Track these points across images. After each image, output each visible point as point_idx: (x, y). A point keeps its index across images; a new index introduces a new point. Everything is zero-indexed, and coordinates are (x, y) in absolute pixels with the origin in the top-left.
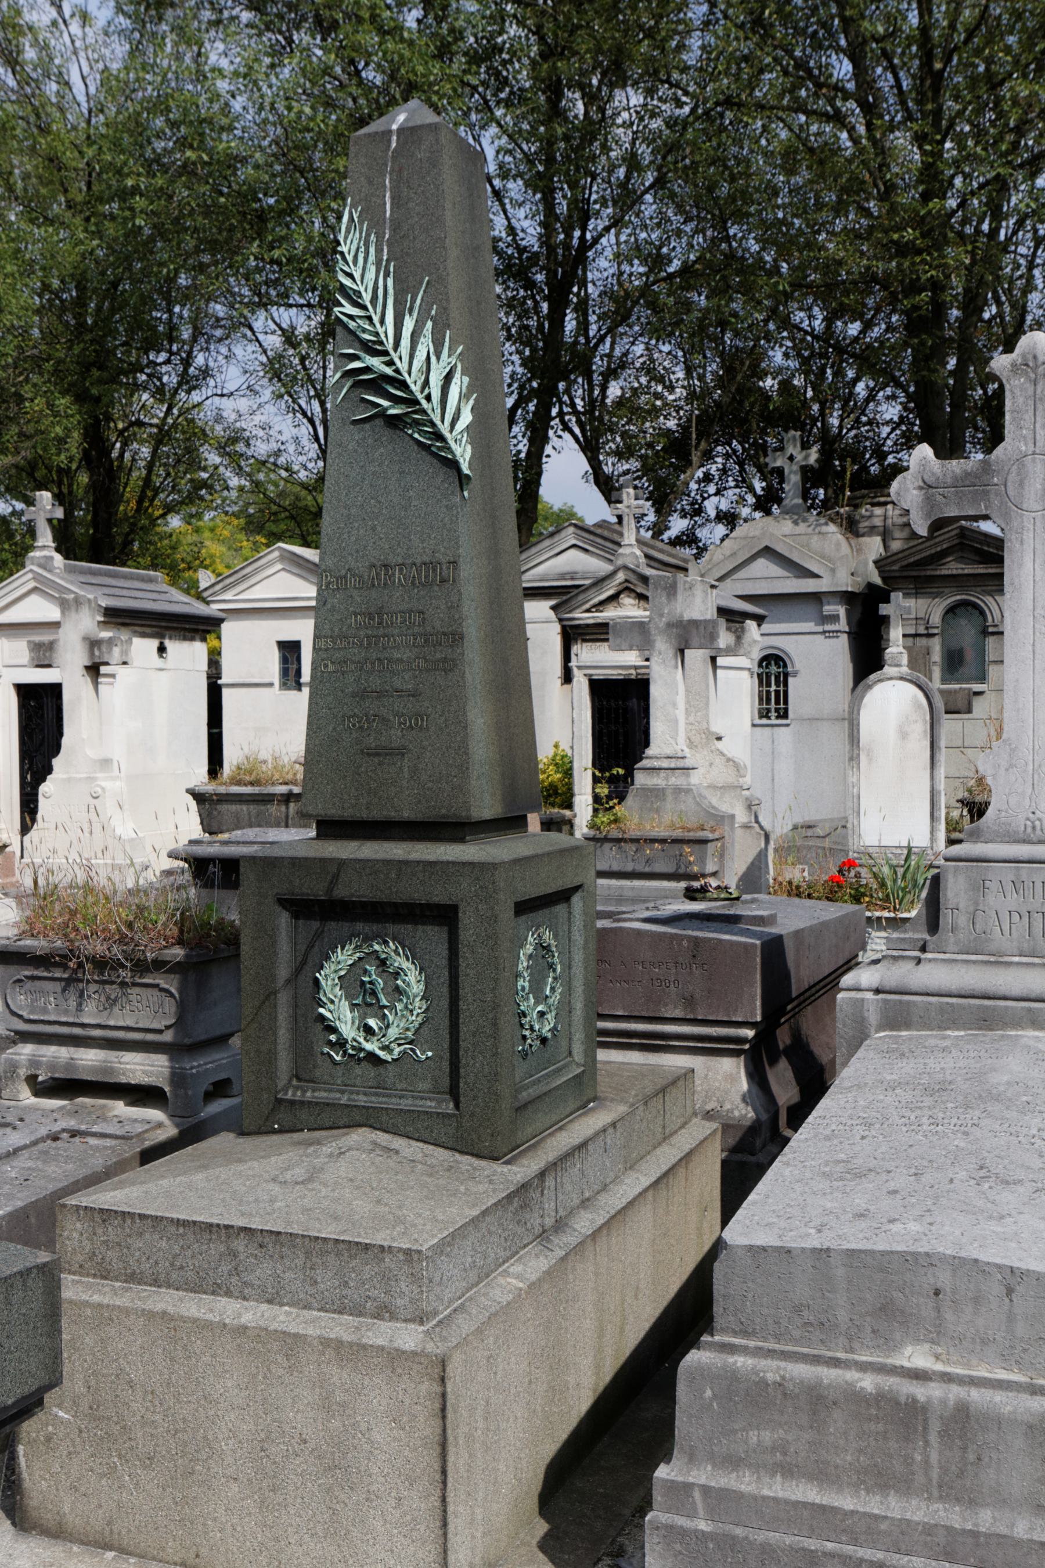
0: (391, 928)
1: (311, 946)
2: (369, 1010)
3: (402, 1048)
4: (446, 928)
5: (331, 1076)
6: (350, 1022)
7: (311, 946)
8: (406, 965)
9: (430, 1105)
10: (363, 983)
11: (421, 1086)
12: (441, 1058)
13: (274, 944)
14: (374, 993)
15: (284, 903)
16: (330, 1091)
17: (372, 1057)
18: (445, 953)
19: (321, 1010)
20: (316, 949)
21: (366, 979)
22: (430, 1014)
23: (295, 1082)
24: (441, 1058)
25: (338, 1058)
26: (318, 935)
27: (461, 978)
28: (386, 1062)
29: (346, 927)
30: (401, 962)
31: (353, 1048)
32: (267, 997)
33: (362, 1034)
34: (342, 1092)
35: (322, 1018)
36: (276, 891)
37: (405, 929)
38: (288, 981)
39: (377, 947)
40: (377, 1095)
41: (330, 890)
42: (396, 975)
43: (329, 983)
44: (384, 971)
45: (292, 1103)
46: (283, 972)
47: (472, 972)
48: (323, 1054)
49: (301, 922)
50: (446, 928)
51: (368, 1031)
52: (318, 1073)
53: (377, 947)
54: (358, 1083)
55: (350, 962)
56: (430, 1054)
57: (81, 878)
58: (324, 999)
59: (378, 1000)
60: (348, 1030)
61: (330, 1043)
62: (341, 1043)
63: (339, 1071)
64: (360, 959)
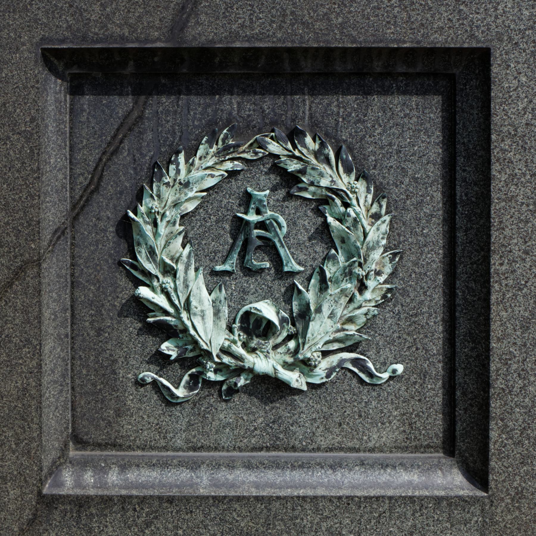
0: (306, 106)
1: (112, 151)
2: (251, 284)
3: (334, 359)
4: (436, 100)
5: (159, 429)
6: (210, 313)
7: (112, 151)
8: (344, 182)
9: (405, 480)
10: (240, 225)
11: (376, 436)
12: (424, 374)
13: (35, 152)
14: (269, 248)
15: (54, 59)
16: (164, 464)
17: (270, 388)
18: (436, 153)
19: (144, 292)
20: (124, 157)
21: (252, 217)
22: (397, 284)
23: (73, 453)
24: (424, 374)
25: (180, 392)
26: (130, 126)
27: (496, 206)
28: (299, 392)
29: (197, 107)
30: (330, 177)
31: (220, 368)
32: (19, 273)
33: (238, 335)
34: (194, 465)
35: (143, 308)
36: (39, 33)
37: (339, 107)
38: (59, 233)
39: (274, 147)
40: (276, 465)
41: (179, 25)
42: (322, 202)
43: (163, 229)
44: (289, 196)
45: (81, 503)
46: (53, 213)
47: (521, 193)
48: (140, 383)
49: (86, 100)
50: (436, 100)
51: (256, 329)
52: (126, 427)
53: (274, 147)
54: (224, 441)
55: (210, 182)
56: (400, 368)
57: (251, 366)
58: (150, 267)
59: (277, 261)
60: (211, 332)
61: (161, 360)
62: (195, 357)
63: (181, 418)
64: (232, 174)
